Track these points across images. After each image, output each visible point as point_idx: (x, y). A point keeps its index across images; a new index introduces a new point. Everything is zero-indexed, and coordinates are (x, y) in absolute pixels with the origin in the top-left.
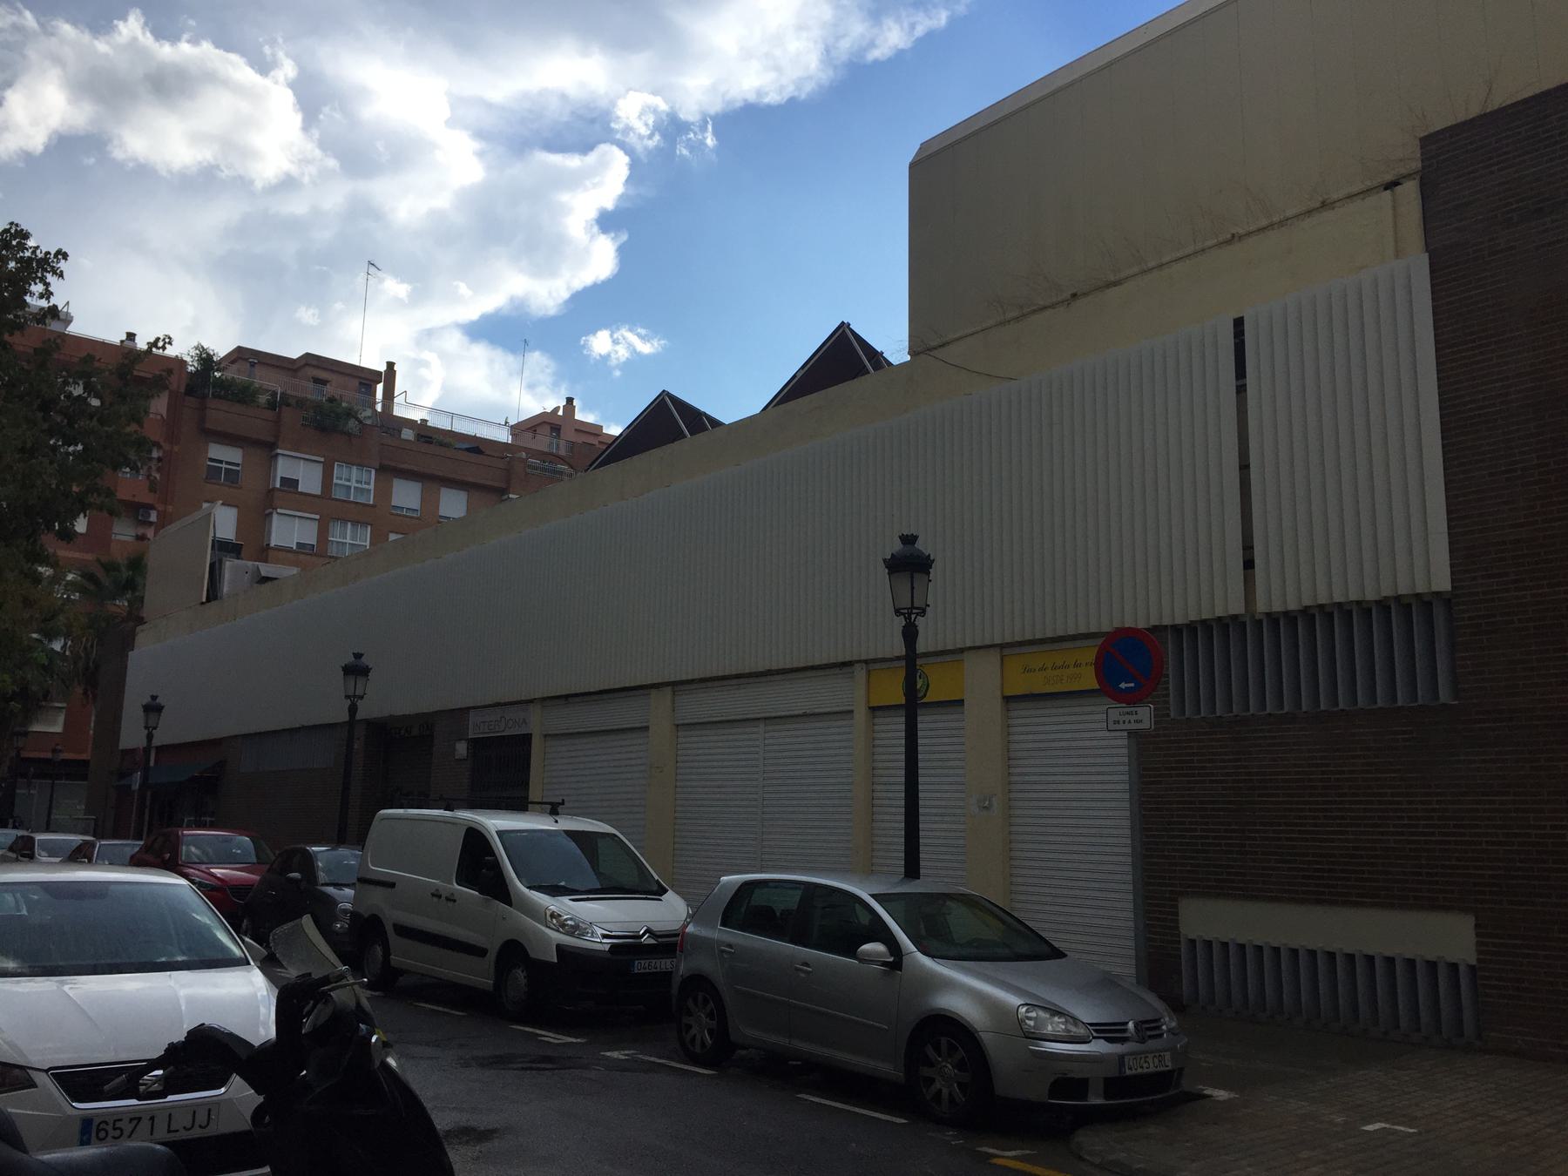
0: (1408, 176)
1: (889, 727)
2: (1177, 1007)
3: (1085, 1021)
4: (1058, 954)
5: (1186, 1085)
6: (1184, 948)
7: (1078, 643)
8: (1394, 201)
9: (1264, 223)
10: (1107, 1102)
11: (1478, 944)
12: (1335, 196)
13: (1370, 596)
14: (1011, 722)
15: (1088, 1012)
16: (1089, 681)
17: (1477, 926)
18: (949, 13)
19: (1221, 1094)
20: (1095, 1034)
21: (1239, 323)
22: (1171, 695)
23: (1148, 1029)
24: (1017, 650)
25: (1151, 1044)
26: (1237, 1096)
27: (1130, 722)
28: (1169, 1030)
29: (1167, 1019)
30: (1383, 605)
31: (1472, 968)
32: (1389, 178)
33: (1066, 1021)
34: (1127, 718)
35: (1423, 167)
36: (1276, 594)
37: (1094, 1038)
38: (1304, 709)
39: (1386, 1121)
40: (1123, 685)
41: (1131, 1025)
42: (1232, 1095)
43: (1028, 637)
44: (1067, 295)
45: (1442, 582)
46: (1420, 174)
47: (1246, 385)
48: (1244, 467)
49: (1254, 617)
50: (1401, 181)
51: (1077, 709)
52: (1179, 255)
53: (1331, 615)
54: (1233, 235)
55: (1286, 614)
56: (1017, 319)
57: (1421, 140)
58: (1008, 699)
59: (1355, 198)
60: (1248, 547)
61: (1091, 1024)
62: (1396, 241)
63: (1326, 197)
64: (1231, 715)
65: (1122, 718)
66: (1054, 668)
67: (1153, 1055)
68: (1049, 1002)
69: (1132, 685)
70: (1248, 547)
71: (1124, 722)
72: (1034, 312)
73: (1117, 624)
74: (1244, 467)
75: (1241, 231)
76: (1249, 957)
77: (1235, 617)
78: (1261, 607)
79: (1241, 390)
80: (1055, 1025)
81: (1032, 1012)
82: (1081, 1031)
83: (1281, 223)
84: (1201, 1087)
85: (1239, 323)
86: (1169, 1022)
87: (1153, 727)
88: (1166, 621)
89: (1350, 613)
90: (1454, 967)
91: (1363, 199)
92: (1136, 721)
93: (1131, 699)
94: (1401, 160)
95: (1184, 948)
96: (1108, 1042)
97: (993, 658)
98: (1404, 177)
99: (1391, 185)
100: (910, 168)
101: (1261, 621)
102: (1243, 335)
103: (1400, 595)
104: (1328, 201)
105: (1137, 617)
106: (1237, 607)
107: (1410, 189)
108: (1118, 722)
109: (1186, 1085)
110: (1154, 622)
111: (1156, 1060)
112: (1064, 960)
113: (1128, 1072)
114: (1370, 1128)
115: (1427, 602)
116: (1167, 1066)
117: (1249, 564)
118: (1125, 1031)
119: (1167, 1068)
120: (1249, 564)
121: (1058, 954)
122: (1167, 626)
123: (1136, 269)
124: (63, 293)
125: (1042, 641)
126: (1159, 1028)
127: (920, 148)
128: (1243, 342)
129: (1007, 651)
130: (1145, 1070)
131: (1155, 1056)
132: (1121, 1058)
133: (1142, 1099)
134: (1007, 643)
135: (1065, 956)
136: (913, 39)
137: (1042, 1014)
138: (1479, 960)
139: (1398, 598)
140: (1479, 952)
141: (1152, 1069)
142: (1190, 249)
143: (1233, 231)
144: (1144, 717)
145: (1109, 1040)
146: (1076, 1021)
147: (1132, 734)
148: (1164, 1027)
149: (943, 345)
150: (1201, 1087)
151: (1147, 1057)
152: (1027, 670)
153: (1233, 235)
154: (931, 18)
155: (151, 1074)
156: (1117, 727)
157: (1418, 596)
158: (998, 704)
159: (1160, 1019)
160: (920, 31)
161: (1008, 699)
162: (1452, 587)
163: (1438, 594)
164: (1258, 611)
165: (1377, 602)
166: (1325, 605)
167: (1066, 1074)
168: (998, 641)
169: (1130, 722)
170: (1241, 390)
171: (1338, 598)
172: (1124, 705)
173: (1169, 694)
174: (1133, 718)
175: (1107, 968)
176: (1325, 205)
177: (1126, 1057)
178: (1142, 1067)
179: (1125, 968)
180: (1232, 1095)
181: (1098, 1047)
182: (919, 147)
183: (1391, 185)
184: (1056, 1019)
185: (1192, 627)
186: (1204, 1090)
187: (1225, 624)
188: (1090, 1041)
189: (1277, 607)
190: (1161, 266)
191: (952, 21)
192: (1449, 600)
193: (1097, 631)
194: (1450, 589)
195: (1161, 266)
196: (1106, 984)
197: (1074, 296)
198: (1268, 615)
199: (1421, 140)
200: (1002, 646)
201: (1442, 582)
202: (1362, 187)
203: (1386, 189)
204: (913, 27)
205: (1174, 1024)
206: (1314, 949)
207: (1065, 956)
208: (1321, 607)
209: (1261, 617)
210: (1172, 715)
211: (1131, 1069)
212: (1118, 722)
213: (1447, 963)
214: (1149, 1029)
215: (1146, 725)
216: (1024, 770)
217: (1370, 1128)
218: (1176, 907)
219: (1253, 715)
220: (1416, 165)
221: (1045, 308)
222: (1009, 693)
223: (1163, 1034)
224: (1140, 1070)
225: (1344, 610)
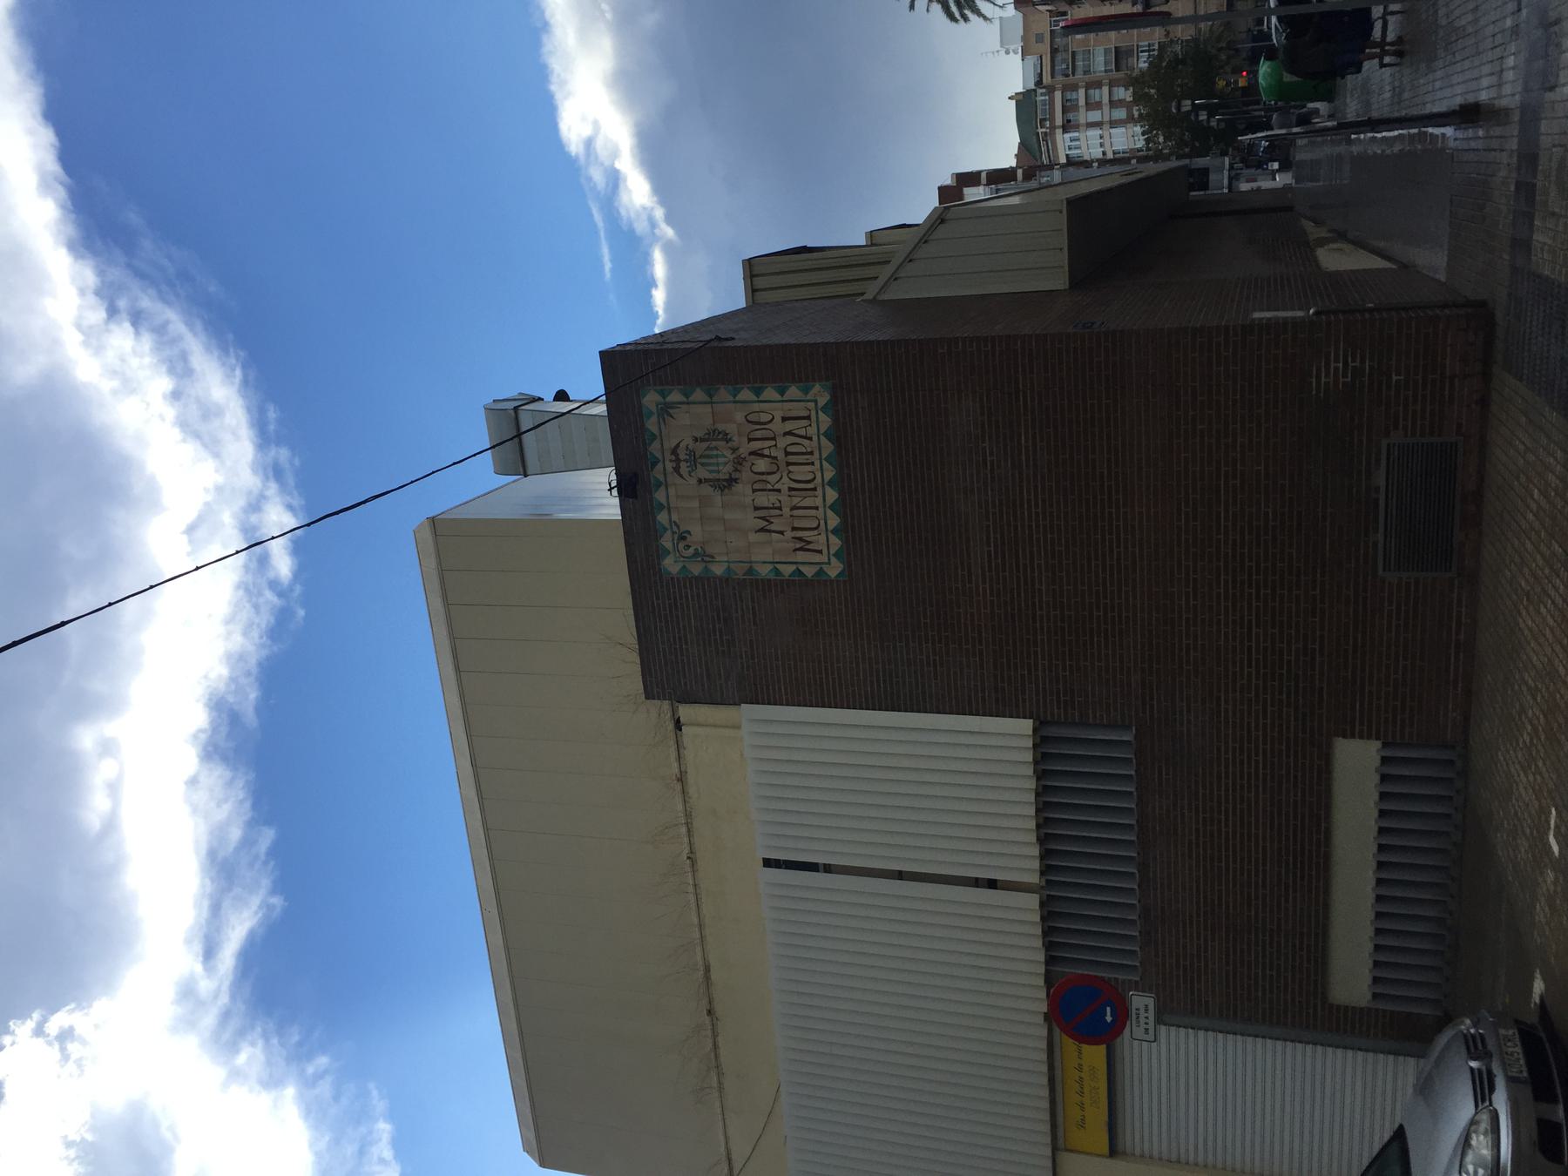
0: (674, 712)
1: (1182, 1072)
2: (1446, 1020)
3: (1473, 1111)
4: (1400, 1135)
5: (1533, 1019)
6: (1382, 1006)
7: (1057, 1064)
8: (692, 724)
9: (684, 830)
10: (1561, 1100)
11: (1361, 737)
12: (677, 770)
13: (1032, 784)
14: (1138, 1151)
15: (1463, 1108)
16: (1095, 1054)
17: (1345, 737)
18: (381, 1120)
19: (1538, 986)
20: (1487, 1103)
21: (768, 863)
22: (1116, 976)
23: (1476, 1047)
24: (1060, 1133)
25: (1491, 1044)
26: (1538, 971)
27: (1147, 1018)
28: (1475, 1025)
29: (1463, 1027)
30: (1040, 775)
31: (1385, 745)
32: (671, 726)
33: (1475, 1132)
34: (1142, 1020)
35: (670, 699)
36: (1024, 863)
37: (1491, 1104)
38: (1135, 855)
39: (1547, 835)
40: (1109, 1019)
41: (1473, 1064)
42: (1538, 975)
43: (1047, 1117)
44: (707, 1020)
45: (1026, 726)
46: (674, 702)
47: (825, 864)
48: (900, 875)
49: (1042, 887)
50: (676, 717)
51: (1127, 1082)
52: (694, 906)
53: (1047, 819)
54: (688, 858)
55: (1042, 858)
56: (720, 1075)
57: (647, 698)
58: (1114, 1152)
59: (682, 756)
60: (977, 883)
61: (1476, 1106)
62: (727, 727)
63: (674, 777)
64: (1138, 923)
65: (1143, 1026)
66: (1081, 1094)
67: (1503, 1047)
68: (1455, 1150)
69: (1108, 1009)
70: (977, 883)
71: (1146, 1024)
72: (717, 1057)
73: (1040, 1019)
74: (900, 875)
75: (687, 850)
76: (1388, 926)
77: (1042, 904)
78: (1034, 879)
79: (828, 869)
80: (1480, 1143)
81: (1467, 1170)
82: (1485, 1118)
83: (688, 815)
84: (1532, 1005)
85: (768, 863)
86: (1466, 1025)
87: (1153, 995)
88: (1042, 969)
89: (1045, 803)
90: (1385, 760)
91: (685, 749)
92: (1146, 1011)
93: (1123, 1015)
94: (659, 715)
95: (1382, 1006)
96: (1494, 1091)
97: (1069, 1161)
98: (674, 715)
99: (678, 725)
100: (544, 1167)
101: (1048, 881)
102: (779, 860)
103: (1034, 760)
104: (679, 776)
105: (1039, 1004)
106: (1033, 901)
107: (685, 711)
108: (1147, 1030)
109: (1533, 1019)
110: (1041, 982)
111: (1509, 1044)
112: (1406, 1127)
113: (1525, 1074)
114: (1556, 848)
115: (1042, 744)
116: (1514, 1033)
117: (992, 884)
118: (1480, 1070)
119: (1517, 1033)
120: (992, 884)
121: (1400, 1135)
122: (1046, 970)
123: (699, 949)
124: (1046, 1011)
125: (1053, 1102)
126: (1473, 1036)
127: (528, 1152)
128: (785, 861)
129: (1061, 1143)
130: (1521, 1056)
131: (1505, 1045)
132: (1511, 1080)
133: (1557, 1081)
134: (1052, 1141)
135: (1401, 1127)
136: (394, 1162)
137: (1469, 1158)
138: (1378, 739)
139: (1036, 762)
140: (1369, 737)
141: (1519, 1049)
142: (692, 898)
143: (685, 858)
144: (1141, 1002)
145: (1492, 1089)
146: (1473, 1122)
147: (1159, 1021)
148: (1472, 1031)
149: (730, 1160)
150: (1532, 1005)
151: (1507, 1053)
152: (1082, 1124)
153: (688, 858)
154: (380, 1140)
155: (1378, 263)
156: (1151, 1031)
157: (1035, 746)
158: (1118, 1165)
159: (1465, 1036)
160: (388, 1154)
161: (1114, 1152)
162: (1030, 718)
163: (1035, 730)
164: (1038, 882)
165: (1038, 779)
166: (1036, 822)
167: (1535, 1142)
168: (1048, 1152)
169: (1147, 1018)
170: (828, 869)
171: (1032, 812)
172: (1128, 1023)
173: (1115, 978)
174: (1143, 1014)
175: (1410, 1090)
176: (681, 779)
177: (1510, 1074)
178: (1518, 1059)
179: (1408, 1070)
180: (1538, 975)
181: (1500, 1101)
182: (526, 1154)
183: (678, 725)
184: (1474, 1142)
185: (1049, 946)
186: (1535, 1003)
187: (1050, 914)
188: (1496, 1110)
189: (1036, 864)
190: (701, 926)
191: (391, 1116)
192: (1041, 723)
193: (1046, 1042)
194: (1032, 720)
195: (701, 926)
196: (1426, 1089)
197: (709, 1012)
198: (1042, 873)
199: (647, 698)
200: (1055, 1149)
201: (1026, 726)
202: (673, 748)
203: (681, 730)
204: (382, 1161)
205: (1468, 1022)
206: (1377, 829)
207: (1401, 1127)
208: (1038, 826)
209: (1043, 880)
210: (1138, 979)
211: (1521, 1072)
212: (1147, 1030)
213: (1381, 765)
214: (1475, 1047)
215: (1151, 1002)
216: (1191, 1148)
217: (1556, 848)
218: (1339, 1007)
219: (1139, 901)
220: (666, 705)
221: (715, 1046)
222: (1106, 1150)
223: (1480, 1033)
224: (1522, 1062)
225: (1042, 807)
